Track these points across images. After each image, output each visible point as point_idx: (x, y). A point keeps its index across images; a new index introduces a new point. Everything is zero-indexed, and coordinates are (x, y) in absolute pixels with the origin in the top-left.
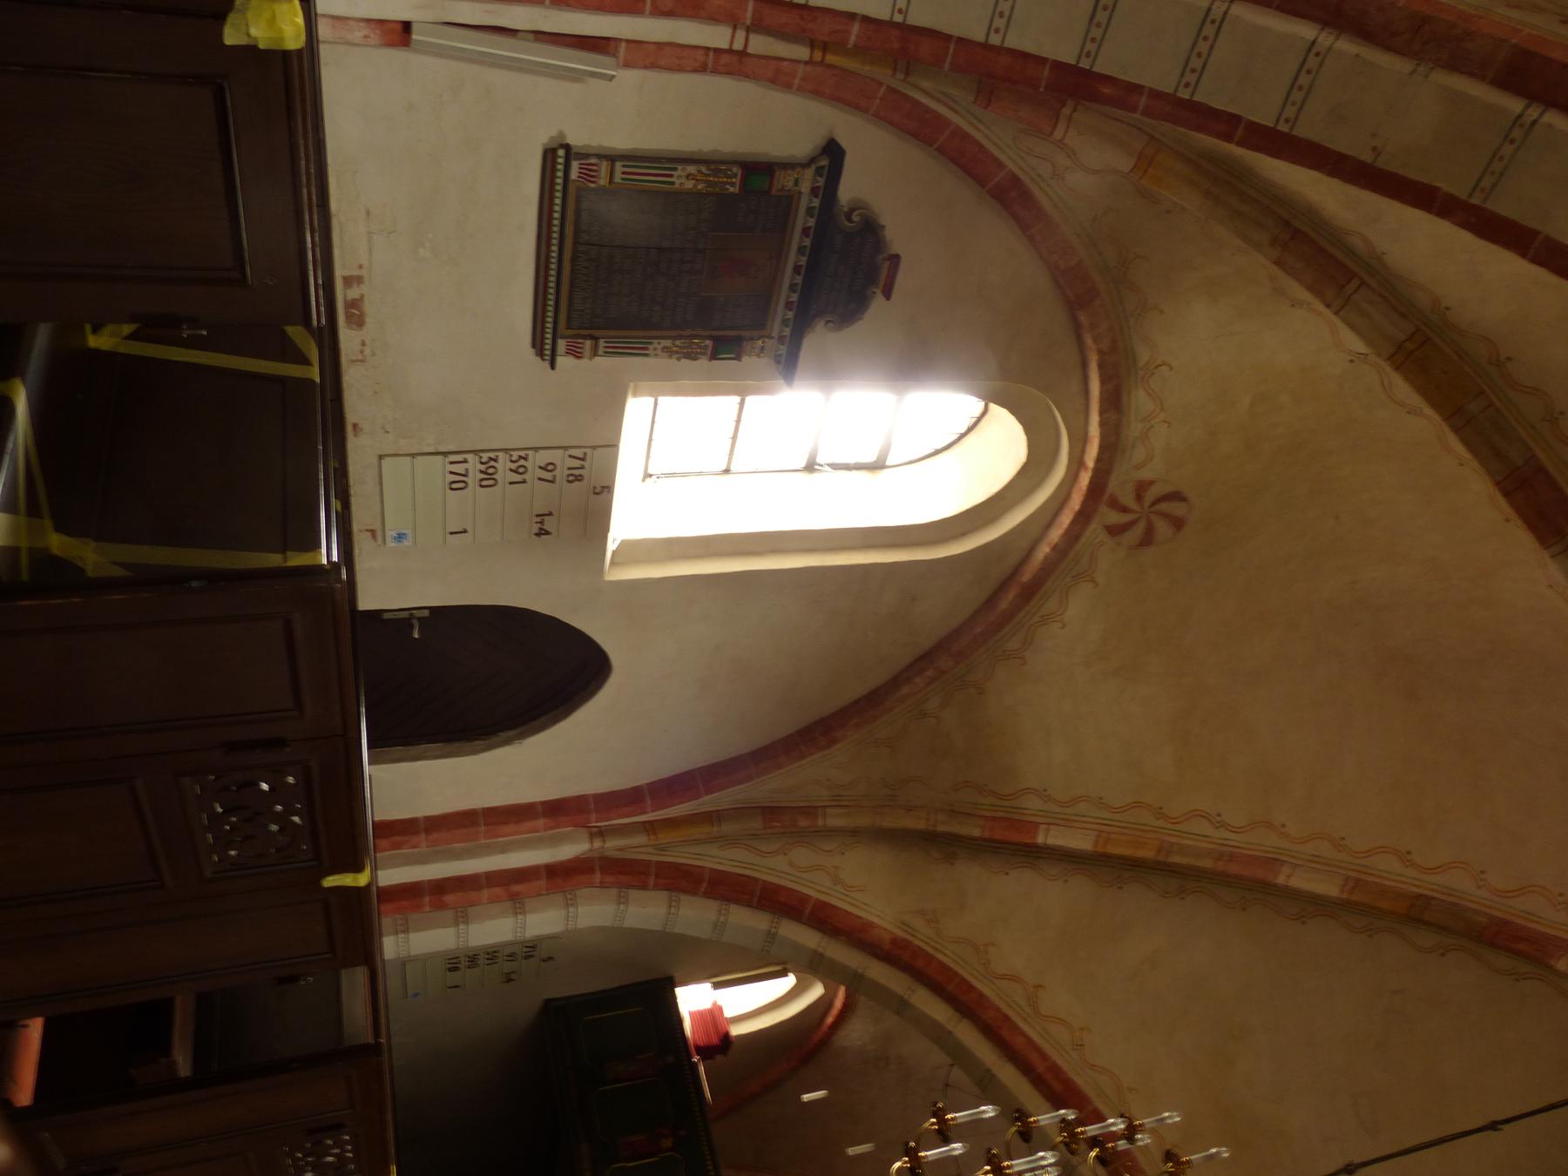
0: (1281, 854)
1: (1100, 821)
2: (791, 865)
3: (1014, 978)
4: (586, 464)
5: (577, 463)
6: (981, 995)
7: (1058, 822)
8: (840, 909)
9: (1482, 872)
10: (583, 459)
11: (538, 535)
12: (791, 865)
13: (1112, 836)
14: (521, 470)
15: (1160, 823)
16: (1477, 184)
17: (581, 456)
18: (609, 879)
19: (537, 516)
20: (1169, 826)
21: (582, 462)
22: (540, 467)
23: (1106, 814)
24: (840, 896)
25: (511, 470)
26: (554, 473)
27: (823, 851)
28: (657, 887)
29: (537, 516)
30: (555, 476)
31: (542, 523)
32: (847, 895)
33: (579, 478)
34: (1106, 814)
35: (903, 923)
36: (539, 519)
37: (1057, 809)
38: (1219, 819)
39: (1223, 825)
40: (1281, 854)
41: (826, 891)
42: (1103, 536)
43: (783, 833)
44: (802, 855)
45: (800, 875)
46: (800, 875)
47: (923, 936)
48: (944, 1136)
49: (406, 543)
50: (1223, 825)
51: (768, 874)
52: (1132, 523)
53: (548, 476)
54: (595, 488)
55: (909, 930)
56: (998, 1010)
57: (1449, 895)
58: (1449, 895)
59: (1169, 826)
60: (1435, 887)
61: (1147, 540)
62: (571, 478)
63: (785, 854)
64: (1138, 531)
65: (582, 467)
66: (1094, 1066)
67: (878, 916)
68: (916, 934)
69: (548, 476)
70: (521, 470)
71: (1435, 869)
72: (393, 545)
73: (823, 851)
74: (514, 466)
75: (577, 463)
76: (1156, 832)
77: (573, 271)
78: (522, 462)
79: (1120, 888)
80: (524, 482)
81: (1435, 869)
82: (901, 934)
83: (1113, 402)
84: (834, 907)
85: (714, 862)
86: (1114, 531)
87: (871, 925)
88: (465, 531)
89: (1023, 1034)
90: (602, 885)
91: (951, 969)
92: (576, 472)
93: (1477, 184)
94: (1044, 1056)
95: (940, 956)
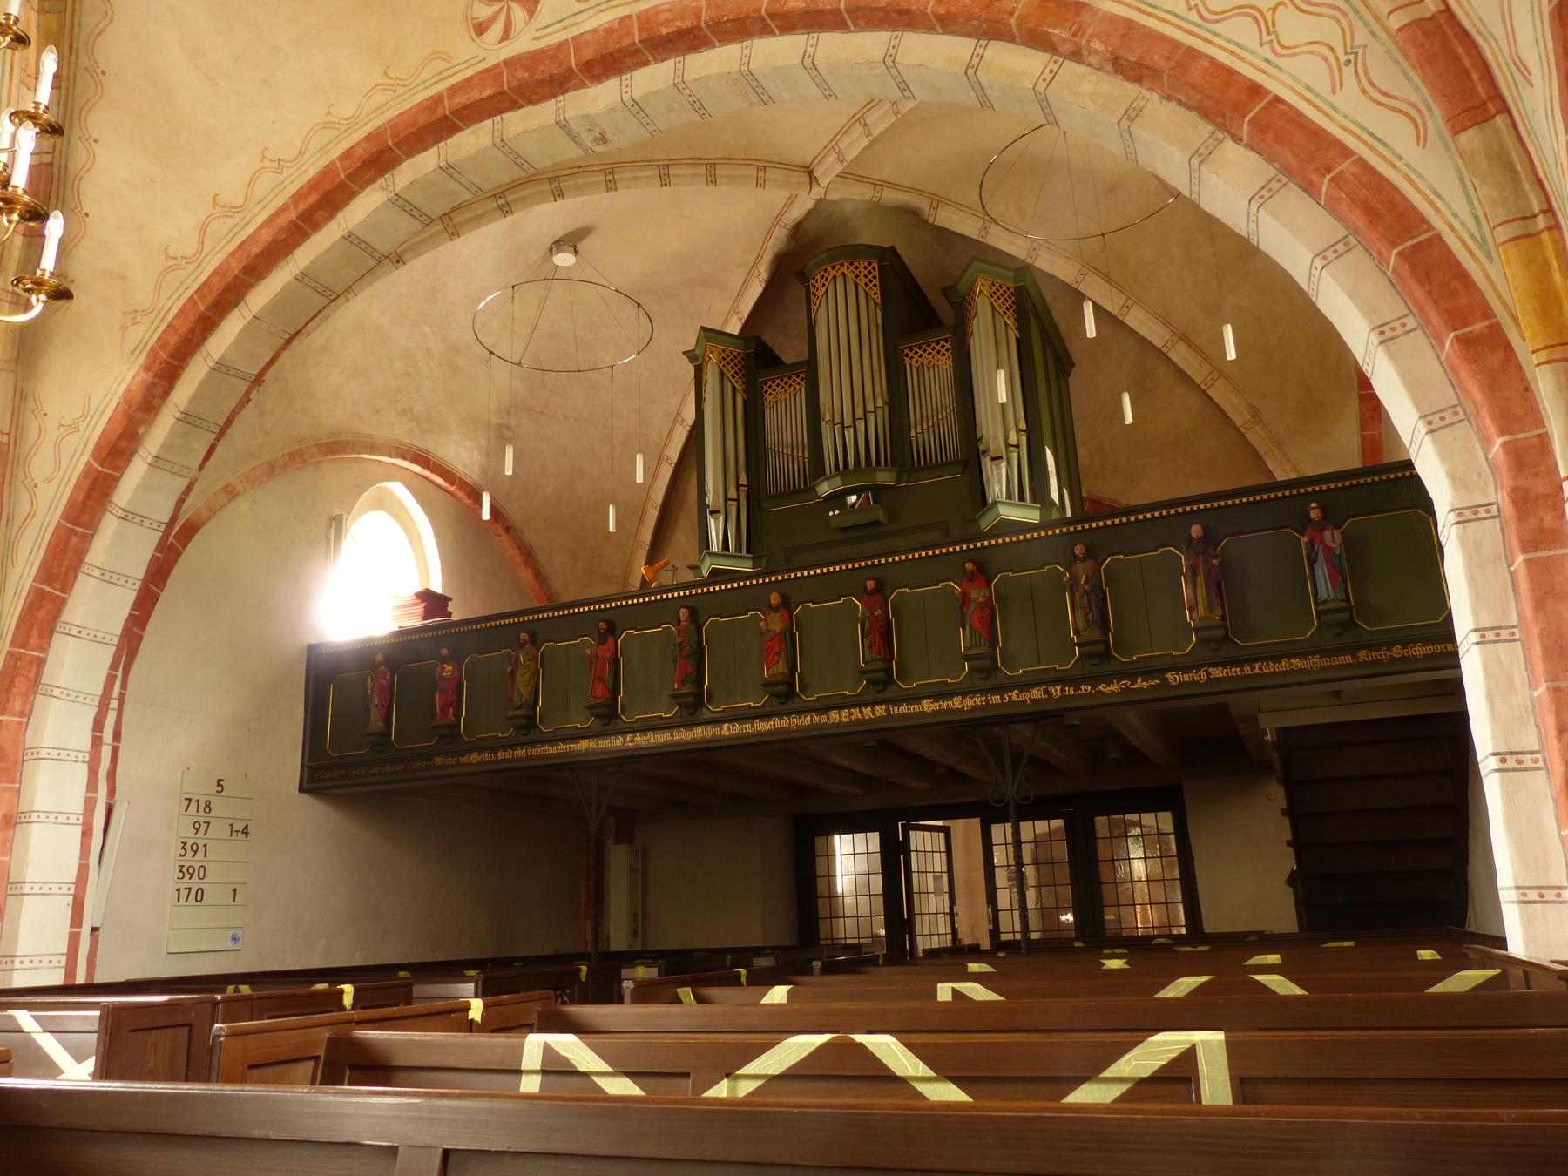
2: (48, 481)
3: (203, 230)
4: (195, 798)
5: (194, 804)
6: (216, 273)
10: (190, 800)
11: (247, 833)
12: (48, 481)
14: (195, 848)
17: (188, 801)
18: (17, 704)
19: (231, 835)
21: (194, 801)
22: (194, 856)
24: (91, 425)
25: (190, 878)
26: (202, 823)
27: (40, 435)
29: (231, 835)
30: (205, 822)
31: (237, 831)
32: (92, 418)
33: (208, 804)
35: (132, 354)
36: (234, 834)
41: (84, 440)
43: (10, 484)
44: (40, 465)
45: (62, 471)
46: (62, 471)
47: (147, 333)
49: (240, 935)
51: (54, 512)
53: (204, 826)
54: (217, 792)
56: (232, 254)
62: (207, 810)
63: (36, 486)
65: (198, 801)
66: (300, 152)
69: (204, 826)
70: (195, 848)
72: (240, 944)
73: (40, 435)
74: (187, 876)
75: (194, 804)
77: (1419, 236)
78: (185, 870)
80: (205, 845)
82: (142, 359)
83: (373, 449)
85: (28, 575)
87: (127, 391)
88: (235, 890)
90: (26, 713)
91: (185, 305)
92: (202, 805)
94: (284, 209)
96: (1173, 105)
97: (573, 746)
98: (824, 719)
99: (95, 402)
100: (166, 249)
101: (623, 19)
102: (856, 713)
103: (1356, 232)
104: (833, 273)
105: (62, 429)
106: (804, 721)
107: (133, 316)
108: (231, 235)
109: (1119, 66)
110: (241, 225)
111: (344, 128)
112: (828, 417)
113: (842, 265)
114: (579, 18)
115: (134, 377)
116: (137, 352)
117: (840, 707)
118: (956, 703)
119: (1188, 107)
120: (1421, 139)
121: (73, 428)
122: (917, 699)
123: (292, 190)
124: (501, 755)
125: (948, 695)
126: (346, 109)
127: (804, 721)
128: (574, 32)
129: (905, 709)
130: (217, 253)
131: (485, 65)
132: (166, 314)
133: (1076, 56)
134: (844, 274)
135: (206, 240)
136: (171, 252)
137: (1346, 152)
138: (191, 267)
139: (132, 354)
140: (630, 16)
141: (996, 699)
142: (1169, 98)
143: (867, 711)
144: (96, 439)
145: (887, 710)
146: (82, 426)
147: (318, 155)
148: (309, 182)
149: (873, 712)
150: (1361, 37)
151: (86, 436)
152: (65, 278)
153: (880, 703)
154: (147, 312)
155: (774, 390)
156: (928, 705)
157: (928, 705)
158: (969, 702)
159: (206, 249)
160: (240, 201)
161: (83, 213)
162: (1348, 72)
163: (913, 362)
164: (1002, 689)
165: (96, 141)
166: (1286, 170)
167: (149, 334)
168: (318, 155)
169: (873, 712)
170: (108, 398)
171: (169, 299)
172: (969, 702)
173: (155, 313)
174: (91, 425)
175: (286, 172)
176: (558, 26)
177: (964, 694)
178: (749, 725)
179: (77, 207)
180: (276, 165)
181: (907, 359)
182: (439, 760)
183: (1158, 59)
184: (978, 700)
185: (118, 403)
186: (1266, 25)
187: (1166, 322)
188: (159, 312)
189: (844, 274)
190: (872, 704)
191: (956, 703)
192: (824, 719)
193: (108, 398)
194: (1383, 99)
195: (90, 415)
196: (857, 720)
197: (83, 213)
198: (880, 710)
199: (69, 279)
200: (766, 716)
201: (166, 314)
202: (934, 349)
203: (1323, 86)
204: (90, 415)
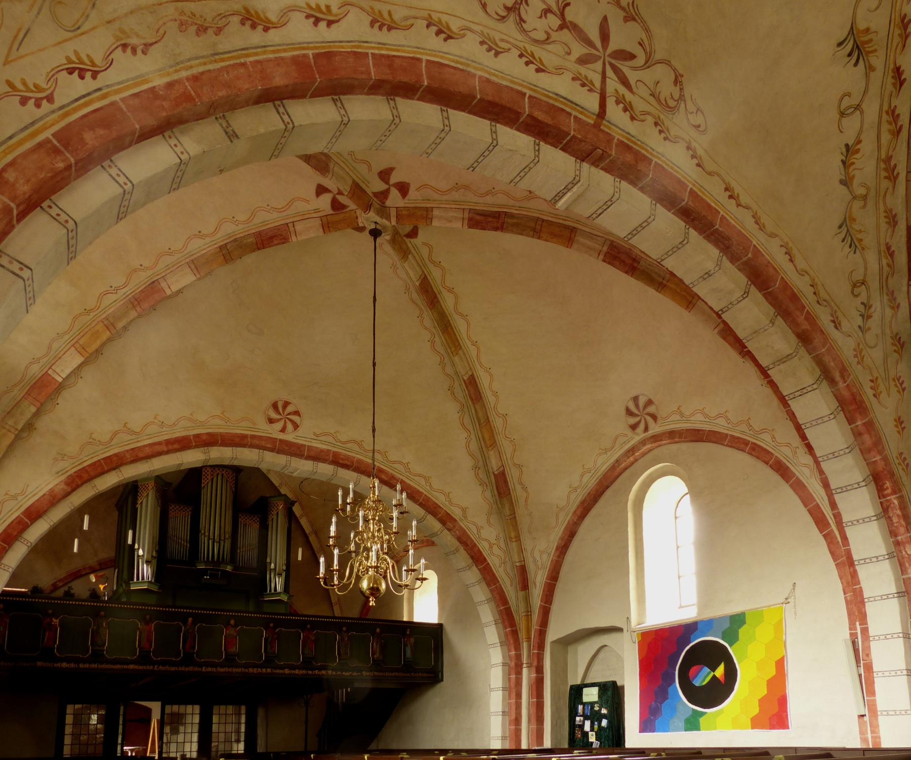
0: (152, 278)
1: (69, 341)
3: (115, 434)
7: (53, 362)
8: (34, 503)
9: (233, 217)
13: (81, 342)
15: (92, 315)
16: (519, 174)
20: (96, 313)
23: (66, 337)
24: (25, 500)
28: (491, 591)
34: (66, 337)
35: (57, 473)
37: (47, 359)
38: (113, 288)
39: (117, 289)
40: (152, 278)
42: (300, 432)
47: (71, 467)
48: (366, 521)
50: (117, 289)
52: (645, 419)
55: (63, 472)
56: (127, 451)
57: (230, 237)
58: (230, 237)
59: (96, 313)
60: (222, 239)
61: (629, 413)
64: (649, 419)
67: (47, 485)
68: (67, 470)
71: (215, 230)
76: (94, 320)
79: (102, 354)
81: (215, 230)
82: (63, 477)
84: (31, 505)
86: (296, 426)
87: (52, 490)
89: (145, 446)
93: (519, 174)
95: (85, 464)
96: (465, 552)
97: (125, 667)
98: (247, 671)
99: (30, 489)
100: (91, 434)
101: (328, 451)
102: (259, 670)
103: (494, 598)
104: (218, 472)
105: (7, 496)
106: (239, 670)
107: (63, 456)
108: (128, 442)
109: (459, 539)
110: (136, 440)
111: (198, 424)
112: (203, 532)
113: (223, 470)
114: (313, 441)
115: (57, 485)
116: (60, 473)
117: (254, 667)
118: (297, 672)
119: (469, 554)
120: (511, 585)
121: (14, 497)
122: (282, 668)
123: (166, 437)
124: (81, 666)
125: (294, 669)
126: (201, 417)
127: (239, 670)
128: (310, 444)
129: (278, 671)
130: (119, 447)
131: (271, 436)
132: (83, 462)
133: (449, 530)
134: (222, 474)
135: (114, 439)
136: (93, 436)
137: (498, 582)
138: (101, 447)
139: (57, 473)
140: (331, 450)
141: (310, 672)
142: (465, 550)
143: (264, 670)
144: (27, 506)
145: (272, 671)
146: (20, 498)
147: (183, 429)
148: (175, 438)
149: (266, 671)
150: (507, 560)
151: (21, 504)
152: (32, 426)
153: (269, 668)
154: (72, 458)
155: (175, 510)
156: (287, 671)
157: (287, 671)
158: (301, 672)
159: (113, 443)
160: (138, 430)
161: (56, 402)
162: (503, 565)
163: (242, 521)
164: (312, 670)
165: (81, 377)
166: (485, 579)
167: (69, 468)
168: (183, 429)
169: (266, 671)
170: (38, 489)
171: (86, 456)
172: (301, 672)
173: (76, 459)
174: (25, 500)
175: (164, 429)
176: (304, 439)
177: (300, 669)
178: (215, 669)
179: (54, 399)
180: (161, 423)
181: (240, 519)
182: (39, 664)
183: (469, 543)
184: (304, 672)
185: (45, 495)
186: (491, 547)
187: (312, 525)
188: (78, 460)
189: (222, 474)
190: (266, 668)
191: (297, 672)
192: (247, 671)
193: (38, 489)
194: (507, 574)
195: (26, 494)
196: (260, 673)
197: (56, 402)
198: (269, 670)
199: (34, 427)
200: (222, 667)
201: (83, 462)
202: (252, 519)
203: (498, 565)
204: (26, 494)
